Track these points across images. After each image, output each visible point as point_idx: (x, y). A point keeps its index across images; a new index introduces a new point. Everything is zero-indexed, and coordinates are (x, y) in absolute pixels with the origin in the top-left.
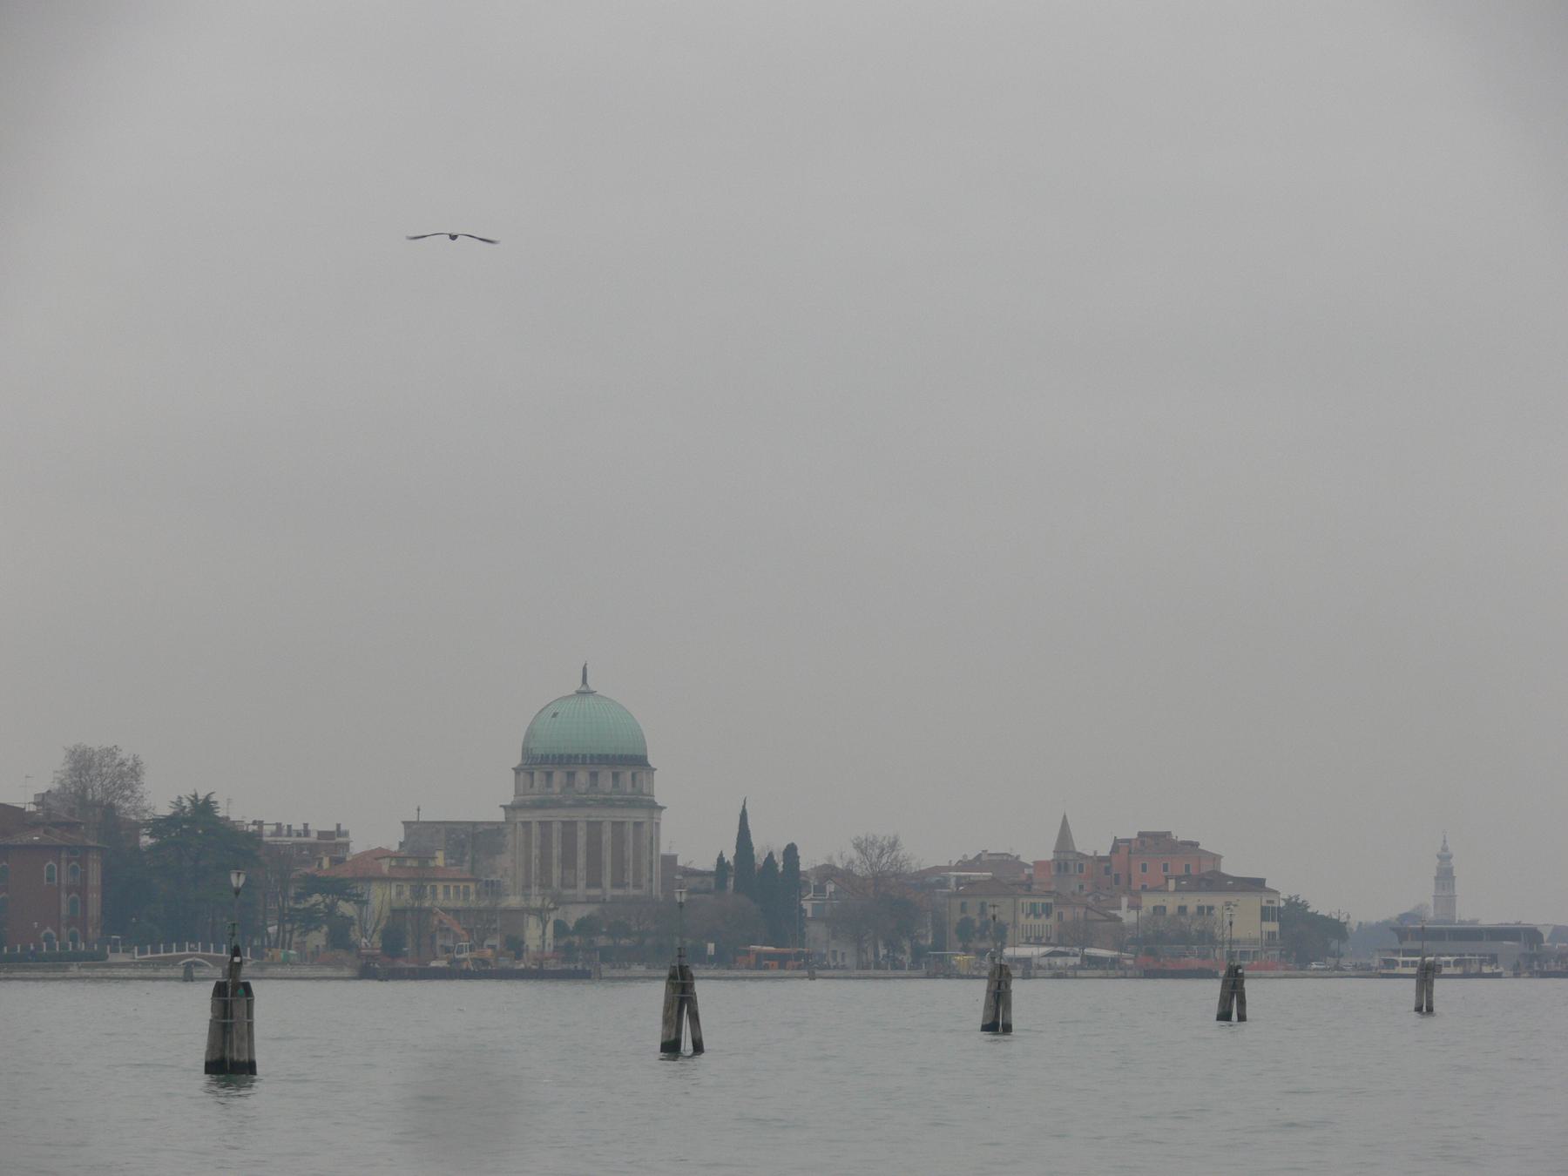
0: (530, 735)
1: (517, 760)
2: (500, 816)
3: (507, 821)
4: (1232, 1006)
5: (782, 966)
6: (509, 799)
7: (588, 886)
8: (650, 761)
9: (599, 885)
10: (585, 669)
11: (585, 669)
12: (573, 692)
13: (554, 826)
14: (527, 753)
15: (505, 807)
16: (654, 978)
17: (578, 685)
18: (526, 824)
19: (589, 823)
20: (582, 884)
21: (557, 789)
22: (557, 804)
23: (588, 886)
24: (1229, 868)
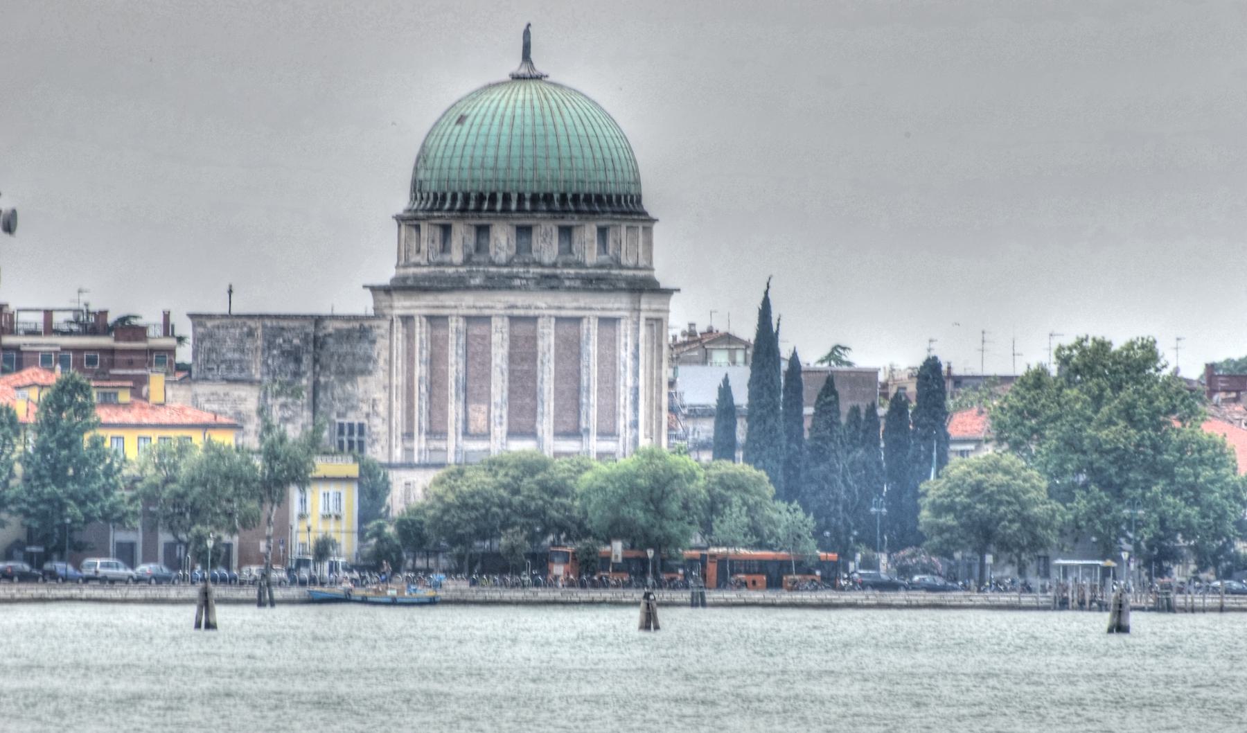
0: (422, 158)
1: (402, 202)
2: (363, 305)
3: (378, 316)
4: (1119, 627)
5: (774, 583)
6: (386, 274)
7: (512, 434)
8: (649, 205)
9: (532, 434)
10: (527, 33)
11: (527, 33)
12: (506, 77)
13: (453, 324)
14: (417, 187)
15: (374, 289)
16: (627, 604)
17: (515, 64)
18: (407, 320)
19: (513, 319)
20: (499, 431)
21: (457, 255)
22: (458, 285)
23: (512, 434)
24: (662, 286)
